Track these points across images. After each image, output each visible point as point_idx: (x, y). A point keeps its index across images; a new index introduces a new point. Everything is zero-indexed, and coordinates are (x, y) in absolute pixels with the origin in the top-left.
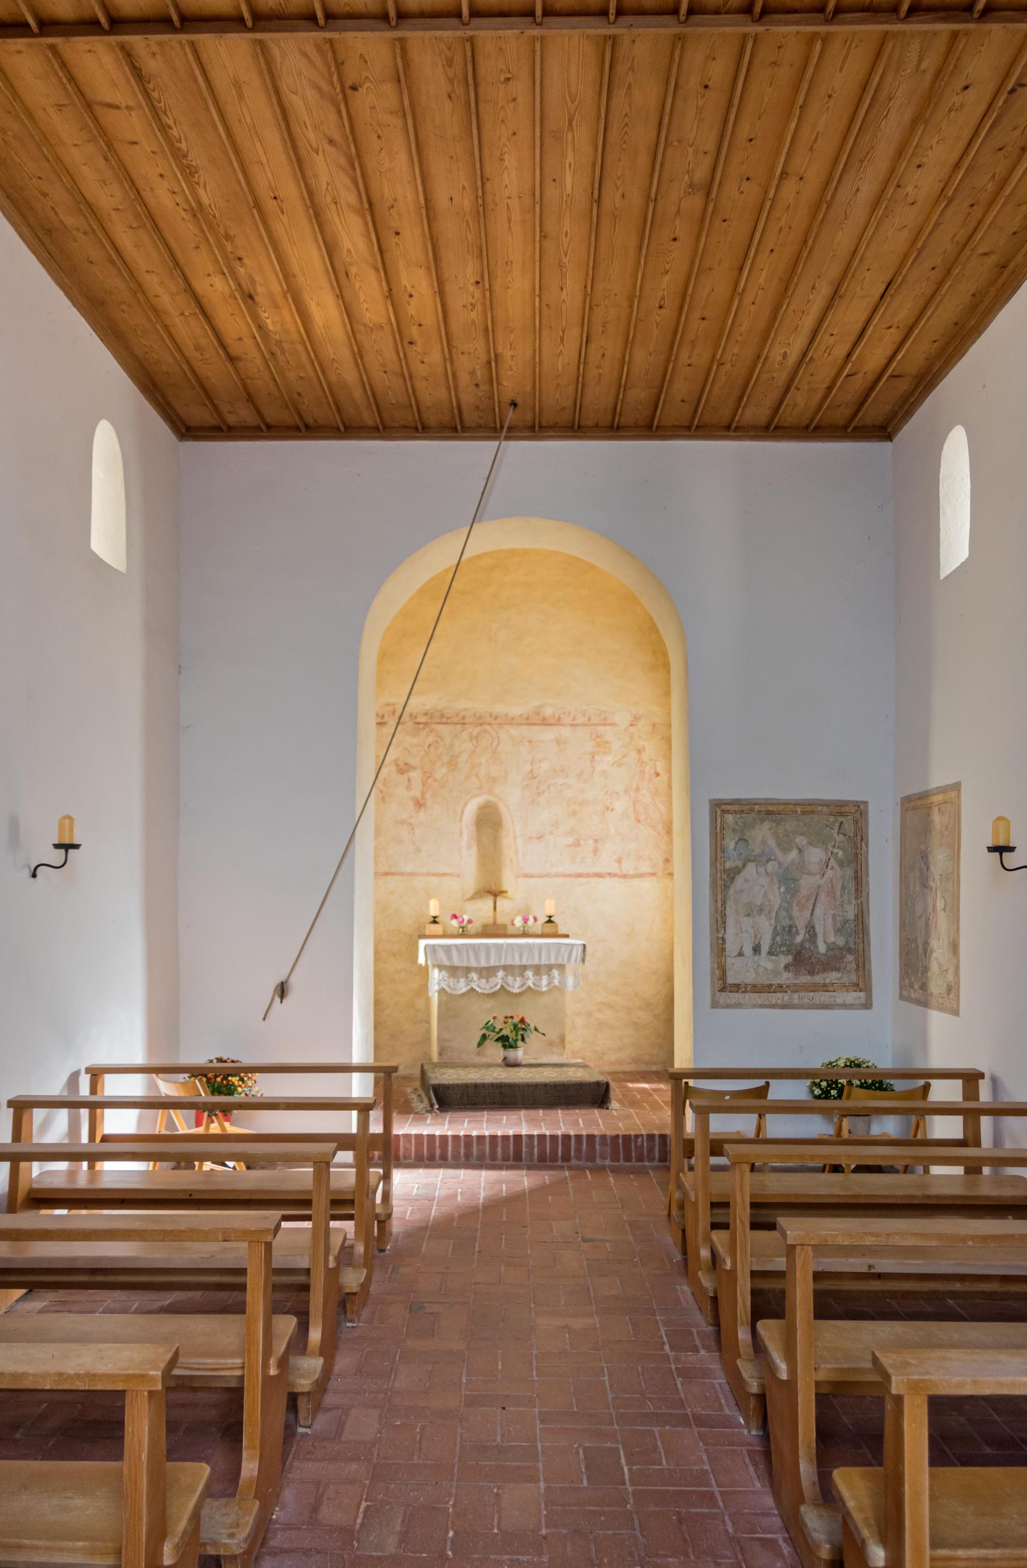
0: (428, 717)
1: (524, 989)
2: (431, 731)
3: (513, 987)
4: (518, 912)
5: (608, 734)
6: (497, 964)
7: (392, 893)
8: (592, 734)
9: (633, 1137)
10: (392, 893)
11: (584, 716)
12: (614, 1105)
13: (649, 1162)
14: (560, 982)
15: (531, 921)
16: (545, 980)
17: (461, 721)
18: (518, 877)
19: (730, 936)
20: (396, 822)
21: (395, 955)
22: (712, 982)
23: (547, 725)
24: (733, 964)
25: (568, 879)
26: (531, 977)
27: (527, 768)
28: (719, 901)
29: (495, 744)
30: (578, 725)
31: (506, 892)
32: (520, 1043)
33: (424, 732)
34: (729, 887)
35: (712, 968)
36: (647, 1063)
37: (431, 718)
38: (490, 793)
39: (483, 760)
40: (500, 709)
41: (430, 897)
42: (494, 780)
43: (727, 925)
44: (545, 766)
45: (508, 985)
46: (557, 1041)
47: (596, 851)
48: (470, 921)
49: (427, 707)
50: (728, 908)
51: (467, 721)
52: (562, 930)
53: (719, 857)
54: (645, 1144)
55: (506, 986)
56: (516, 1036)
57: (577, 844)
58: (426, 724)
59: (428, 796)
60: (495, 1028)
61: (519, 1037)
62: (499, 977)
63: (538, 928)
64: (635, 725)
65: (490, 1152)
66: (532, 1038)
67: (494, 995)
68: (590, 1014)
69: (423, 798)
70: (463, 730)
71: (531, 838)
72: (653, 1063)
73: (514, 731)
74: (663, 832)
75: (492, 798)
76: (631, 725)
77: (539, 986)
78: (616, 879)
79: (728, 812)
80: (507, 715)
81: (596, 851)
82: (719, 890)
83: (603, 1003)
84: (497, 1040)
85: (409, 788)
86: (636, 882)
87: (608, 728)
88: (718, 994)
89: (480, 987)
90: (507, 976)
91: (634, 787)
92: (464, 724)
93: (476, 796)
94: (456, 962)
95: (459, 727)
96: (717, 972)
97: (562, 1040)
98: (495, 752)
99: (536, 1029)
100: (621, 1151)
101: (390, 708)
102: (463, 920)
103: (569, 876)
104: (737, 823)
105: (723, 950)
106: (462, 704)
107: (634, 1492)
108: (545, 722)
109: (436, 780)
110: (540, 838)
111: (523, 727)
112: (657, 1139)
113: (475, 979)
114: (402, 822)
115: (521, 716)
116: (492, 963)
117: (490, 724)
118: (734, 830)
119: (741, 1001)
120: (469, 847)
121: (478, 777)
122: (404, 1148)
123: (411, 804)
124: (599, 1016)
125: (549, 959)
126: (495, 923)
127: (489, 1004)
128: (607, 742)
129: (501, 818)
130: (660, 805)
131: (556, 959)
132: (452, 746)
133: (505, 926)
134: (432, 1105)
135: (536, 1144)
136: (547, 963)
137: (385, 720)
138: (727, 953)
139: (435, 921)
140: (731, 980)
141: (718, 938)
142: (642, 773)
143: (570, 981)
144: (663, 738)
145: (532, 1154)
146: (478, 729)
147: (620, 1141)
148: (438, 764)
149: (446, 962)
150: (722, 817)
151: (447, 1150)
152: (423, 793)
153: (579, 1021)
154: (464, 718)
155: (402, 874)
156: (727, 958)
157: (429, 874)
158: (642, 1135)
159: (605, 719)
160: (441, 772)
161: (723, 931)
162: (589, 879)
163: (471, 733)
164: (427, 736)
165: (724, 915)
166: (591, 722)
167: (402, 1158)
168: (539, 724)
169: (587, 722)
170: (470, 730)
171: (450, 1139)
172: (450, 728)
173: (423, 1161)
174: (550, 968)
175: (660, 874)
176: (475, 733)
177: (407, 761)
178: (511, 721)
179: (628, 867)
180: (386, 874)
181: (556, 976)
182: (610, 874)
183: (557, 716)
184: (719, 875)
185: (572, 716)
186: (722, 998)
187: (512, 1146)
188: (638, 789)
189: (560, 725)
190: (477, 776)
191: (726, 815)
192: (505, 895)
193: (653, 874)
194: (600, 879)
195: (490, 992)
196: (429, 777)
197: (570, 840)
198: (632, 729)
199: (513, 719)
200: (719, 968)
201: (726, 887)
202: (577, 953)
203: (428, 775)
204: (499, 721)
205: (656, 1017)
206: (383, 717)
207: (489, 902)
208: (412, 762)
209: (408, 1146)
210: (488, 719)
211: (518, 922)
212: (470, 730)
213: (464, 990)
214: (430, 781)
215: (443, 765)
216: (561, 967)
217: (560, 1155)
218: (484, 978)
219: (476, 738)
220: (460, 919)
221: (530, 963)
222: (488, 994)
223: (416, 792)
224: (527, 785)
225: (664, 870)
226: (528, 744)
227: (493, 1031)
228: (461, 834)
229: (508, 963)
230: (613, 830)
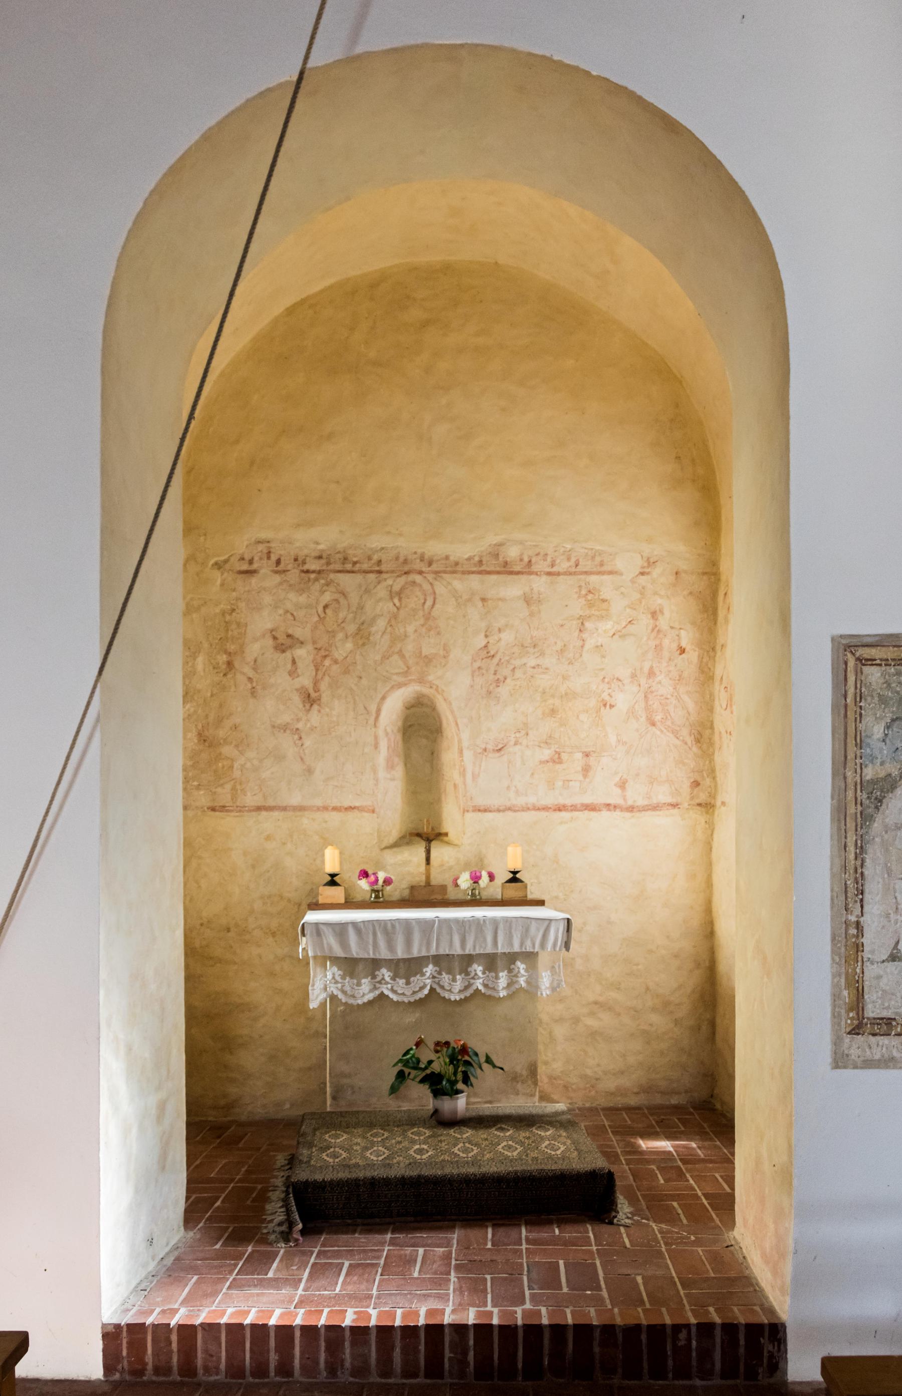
0: (323, 561)
1: (468, 993)
2: (328, 585)
3: (450, 991)
4: (466, 866)
5: (606, 586)
6: (424, 953)
7: (268, 838)
8: (580, 587)
9: (669, 1331)
10: (268, 838)
11: (569, 559)
12: (624, 1208)
13: (702, 1379)
14: (527, 982)
15: (484, 880)
16: (503, 979)
17: (377, 568)
18: (465, 811)
19: (872, 919)
20: (273, 727)
21: (274, 934)
22: (835, 1016)
23: (511, 573)
24: (879, 977)
25: (543, 814)
26: (480, 974)
27: (480, 641)
28: (851, 848)
29: (429, 603)
30: (558, 574)
31: (446, 834)
32: (460, 1086)
33: (317, 586)
34: (871, 818)
35: (835, 986)
36: (663, 1093)
37: (328, 564)
38: (421, 681)
39: (410, 629)
40: (435, 548)
41: (326, 842)
42: (429, 660)
43: (867, 897)
44: (507, 637)
45: (442, 987)
46: (525, 1073)
47: (586, 770)
48: (388, 881)
49: (321, 547)
50: (868, 862)
51: (383, 567)
52: (533, 893)
53: (851, 756)
54: (694, 1343)
55: (439, 990)
56: (455, 1073)
57: (557, 759)
58: (319, 572)
59: (323, 686)
60: (418, 1061)
61: (460, 1076)
62: (428, 974)
63: (495, 890)
64: (648, 573)
65: (378, 1361)
66: (485, 1078)
67: (421, 1002)
68: (576, 1020)
69: (316, 690)
70: (379, 583)
71: (485, 750)
72: (674, 1092)
73: (458, 584)
74: (689, 740)
75: (425, 690)
76: (642, 574)
77: (494, 989)
78: (618, 813)
79: (871, 662)
80: (447, 558)
81: (586, 770)
82: (851, 825)
83: (596, 1003)
84: (422, 1081)
85: (293, 673)
86: (649, 818)
87: (605, 577)
88: (847, 1039)
89: (395, 992)
90: (440, 973)
91: (646, 669)
92: (380, 572)
93: (400, 685)
94: (355, 951)
95: (372, 576)
96: (845, 993)
97: (533, 1071)
98: (428, 617)
99: (488, 1060)
100: (645, 1357)
101: (261, 547)
102: (377, 880)
103: (545, 809)
104: (888, 685)
105: (859, 948)
106: (376, 542)
107: (597, 1249)
108: (506, 569)
109: (336, 662)
110: (500, 750)
111: (472, 576)
112: (718, 1332)
113: (387, 979)
114: (285, 728)
115: (469, 559)
116: (415, 953)
117: (421, 573)
118: (883, 700)
119: (895, 1053)
120: (390, 766)
121: (402, 656)
122: (206, 1351)
123: (297, 699)
124: (590, 1022)
125: (511, 944)
126: (428, 883)
127: (411, 1018)
128: (604, 601)
129: (439, 718)
130: (686, 698)
131: (522, 944)
132: (361, 607)
133: (443, 888)
134: (291, 1224)
135: (471, 1342)
136: (507, 950)
137: (255, 566)
138: (866, 955)
139: (333, 881)
140: (871, 1011)
141: (847, 923)
142: (658, 648)
143: (545, 981)
144: (691, 593)
145: (463, 1362)
146: (402, 580)
147: (644, 1337)
148: (340, 635)
149: (339, 952)
150: (858, 672)
151: (293, 1357)
152: (316, 683)
153: (560, 1031)
154: (379, 562)
155: (284, 809)
156: (867, 964)
157: (325, 808)
158: (688, 1326)
159: (602, 564)
160: (344, 648)
161: (858, 911)
162: (576, 814)
163: (391, 586)
164: (322, 592)
165: (860, 878)
166: (579, 569)
167: (200, 1371)
168: (498, 573)
169: (573, 570)
170: (390, 582)
171: (298, 1334)
172: (359, 578)
173: (244, 1377)
174: (511, 958)
175: (686, 805)
176: (396, 588)
177: (290, 632)
178: (455, 568)
179: (636, 795)
180: (259, 809)
181: (522, 972)
182: (609, 805)
183: (526, 559)
184: (850, 794)
185: (549, 559)
186: (856, 1046)
187: (422, 1347)
188: (651, 674)
189: (531, 573)
190: (401, 653)
191: (867, 670)
192: (445, 839)
193: (674, 806)
194: (593, 814)
195: (412, 1000)
196: (325, 657)
197: (547, 753)
198: (643, 580)
199: (457, 564)
200: (848, 985)
201: (865, 819)
202: (556, 933)
203: (323, 654)
204: (434, 567)
205: (676, 1022)
206: (251, 562)
207: (419, 851)
208: (298, 632)
209: (212, 1348)
210: (418, 565)
211: (465, 881)
212: (390, 582)
213: (370, 996)
214: (327, 662)
215: (347, 637)
216: (530, 957)
217: (520, 1365)
218: (401, 978)
219: (399, 594)
220: (372, 878)
221: (478, 951)
222: (410, 1002)
223: (305, 680)
224: (479, 668)
225: (692, 798)
226: (480, 604)
227: (416, 1068)
228: (376, 746)
229: (441, 952)
230: (613, 739)
